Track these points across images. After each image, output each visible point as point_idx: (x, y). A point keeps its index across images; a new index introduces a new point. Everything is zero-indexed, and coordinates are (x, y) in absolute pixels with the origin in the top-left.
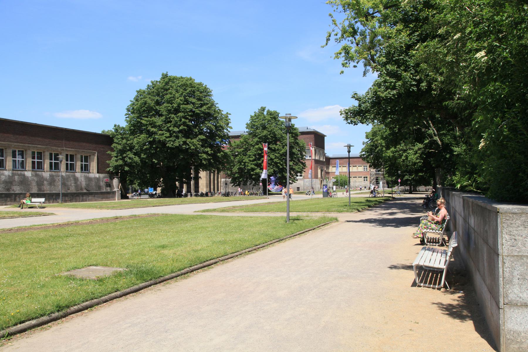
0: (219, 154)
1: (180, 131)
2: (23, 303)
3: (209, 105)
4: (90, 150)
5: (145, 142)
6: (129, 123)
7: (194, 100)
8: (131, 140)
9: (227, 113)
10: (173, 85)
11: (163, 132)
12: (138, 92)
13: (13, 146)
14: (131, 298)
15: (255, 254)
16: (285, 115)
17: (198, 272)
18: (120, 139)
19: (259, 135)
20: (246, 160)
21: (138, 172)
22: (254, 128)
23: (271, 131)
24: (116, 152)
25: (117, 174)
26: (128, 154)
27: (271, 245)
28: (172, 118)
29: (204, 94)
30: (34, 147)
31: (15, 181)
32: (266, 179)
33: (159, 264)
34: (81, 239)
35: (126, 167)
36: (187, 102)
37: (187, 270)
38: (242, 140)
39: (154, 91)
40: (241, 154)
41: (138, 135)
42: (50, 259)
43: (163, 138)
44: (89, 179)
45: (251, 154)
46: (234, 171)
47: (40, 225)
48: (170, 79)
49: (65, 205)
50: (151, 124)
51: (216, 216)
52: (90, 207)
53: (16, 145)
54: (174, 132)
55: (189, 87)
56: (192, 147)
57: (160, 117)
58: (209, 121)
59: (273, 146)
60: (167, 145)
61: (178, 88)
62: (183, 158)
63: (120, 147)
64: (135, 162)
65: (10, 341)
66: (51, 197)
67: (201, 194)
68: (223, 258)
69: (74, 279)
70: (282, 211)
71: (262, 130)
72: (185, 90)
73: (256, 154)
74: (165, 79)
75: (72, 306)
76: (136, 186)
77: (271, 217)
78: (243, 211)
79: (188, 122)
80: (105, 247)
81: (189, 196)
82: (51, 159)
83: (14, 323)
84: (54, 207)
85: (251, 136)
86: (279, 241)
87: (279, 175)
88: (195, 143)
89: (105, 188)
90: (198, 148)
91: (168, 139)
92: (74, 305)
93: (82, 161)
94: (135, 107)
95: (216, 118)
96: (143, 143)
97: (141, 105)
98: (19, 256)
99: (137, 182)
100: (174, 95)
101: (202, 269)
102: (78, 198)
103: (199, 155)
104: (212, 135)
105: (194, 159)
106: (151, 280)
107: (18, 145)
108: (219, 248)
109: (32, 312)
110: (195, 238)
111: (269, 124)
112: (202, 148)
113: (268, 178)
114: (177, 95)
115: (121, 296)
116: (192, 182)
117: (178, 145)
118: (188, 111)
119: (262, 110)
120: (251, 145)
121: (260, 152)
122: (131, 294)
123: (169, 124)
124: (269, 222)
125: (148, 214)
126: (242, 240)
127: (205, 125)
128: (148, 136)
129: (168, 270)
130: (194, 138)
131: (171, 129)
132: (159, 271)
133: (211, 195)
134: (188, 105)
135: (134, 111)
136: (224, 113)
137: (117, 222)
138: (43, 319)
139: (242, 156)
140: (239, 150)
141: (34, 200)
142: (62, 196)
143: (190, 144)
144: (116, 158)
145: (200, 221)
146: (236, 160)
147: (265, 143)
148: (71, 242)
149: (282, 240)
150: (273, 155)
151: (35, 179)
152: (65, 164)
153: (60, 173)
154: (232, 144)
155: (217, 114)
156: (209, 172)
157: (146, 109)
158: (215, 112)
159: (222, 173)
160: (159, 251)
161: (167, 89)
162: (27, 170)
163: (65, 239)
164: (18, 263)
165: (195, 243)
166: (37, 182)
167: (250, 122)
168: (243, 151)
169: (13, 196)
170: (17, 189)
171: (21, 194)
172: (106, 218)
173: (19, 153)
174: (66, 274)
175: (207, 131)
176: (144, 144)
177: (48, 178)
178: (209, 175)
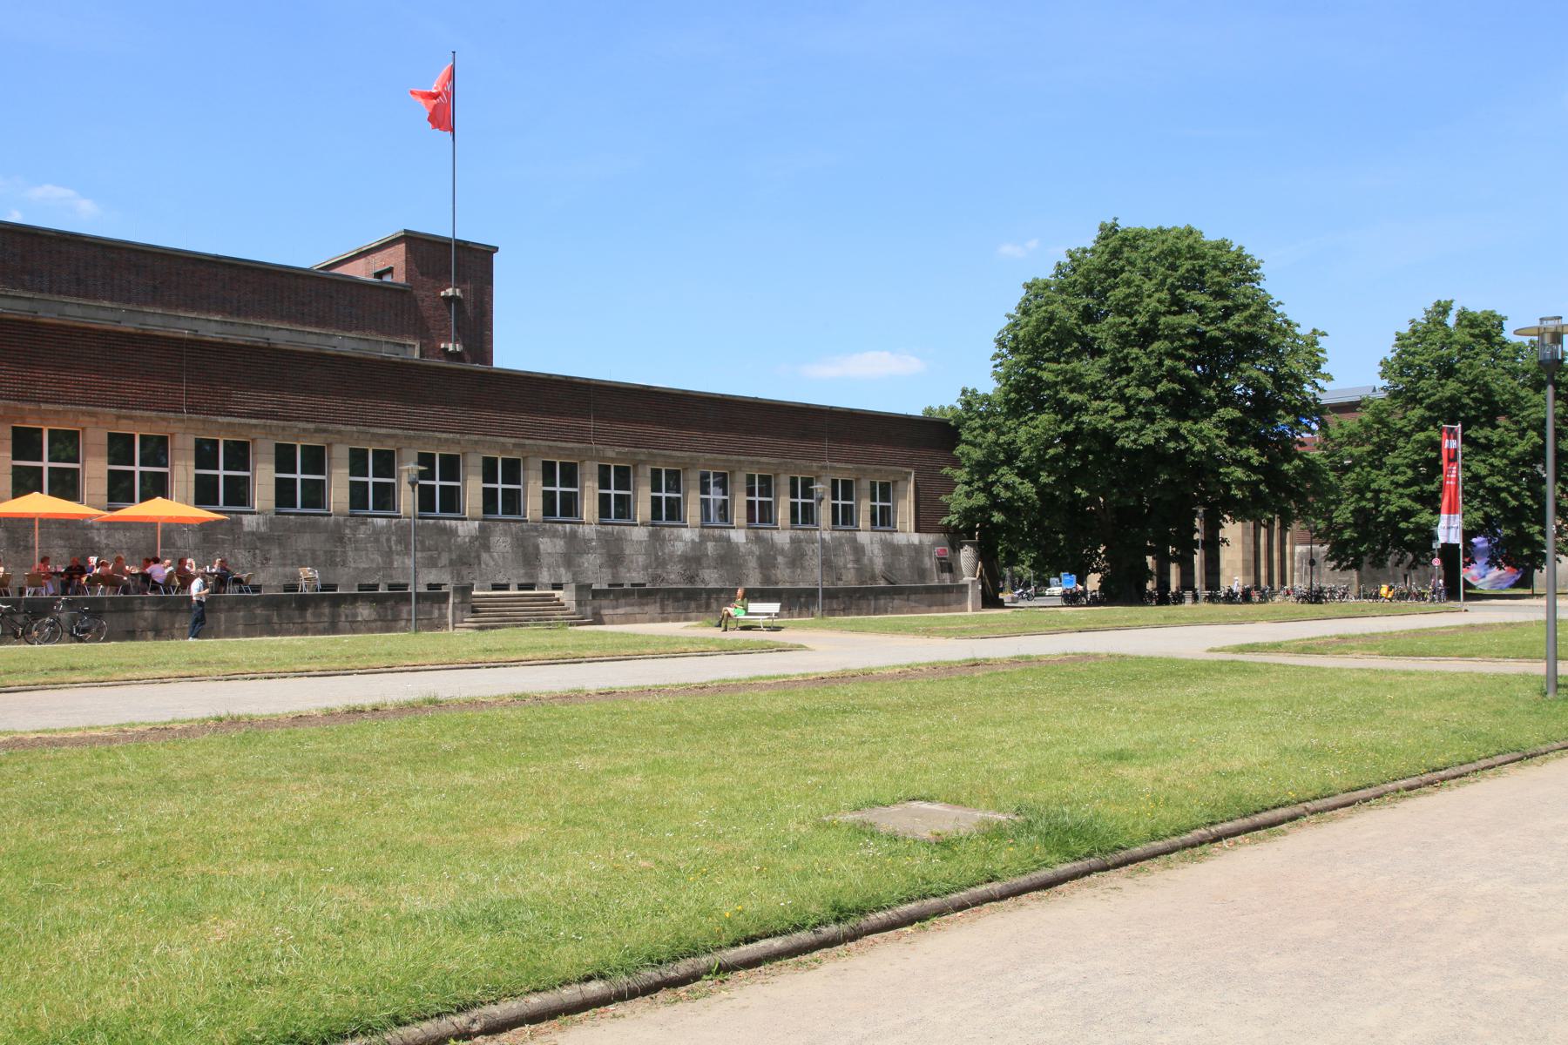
0: (1286, 467)
1: (1160, 399)
2: (751, 890)
3: (1252, 310)
4: (895, 464)
5: (1052, 436)
6: (1004, 381)
7: (1200, 298)
8: (1009, 433)
9: (1314, 330)
10: (1134, 255)
11: (1105, 403)
12: (1028, 287)
13: (702, 461)
14: (1033, 905)
15: (1431, 798)
16: (1537, 323)
17: (1236, 843)
18: (978, 431)
19: (1429, 396)
20: (1382, 481)
21: (1031, 525)
22: (1408, 376)
23: (1473, 381)
24: (967, 470)
25: (969, 532)
26: (1003, 475)
27: (1489, 773)
28: (1133, 359)
29: (1234, 276)
30: (752, 462)
31: (707, 555)
32: (1458, 545)
33: (1110, 810)
34: (882, 718)
35: (995, 514)
36: (1179, 306)
37: (1200, 835)
38: (1366, 416)
39: (1076, 281)
40: (1364, 464)
41: (1031, 415)
42: (806, 773)
43: (1104, 422)
44: (893, 550)
45: (1398, 461)
46: (1339, 520)
47: (774, 677)
48: (1126, 239)
49: (830, 623)
50: (1067, 382)
51: (1286, 666)
52: (897, 630)
53: (708, 460)
54: (1140, 401)
55: (1186, 259)
56: (1199, 447)
57: (1096, 358)
58: (1251, 359)
59: (1480, 434)
60: (1119, 443)
61: (1152, 264)
62: (1171, 481)
63: (977, 454)
64: (1021, 498)
65: (724, 986)
66: (797, 601)
67: (1227, 596)
68: (1318, 804)
69: (872, 835)
70: (1524, 657)
71: (1439, 379)
72: (1173, 267)
73: (1416, 462)
74: (1109, 240)
75: (871, 912)
76: (1025, 570)
77: (1482, 676)
78: (1377, 652)
79: (1185, 368)
80: (950, 748)
81: (1188, 602)
82: (794, 494)
83: (732, 939)
84: (804, 627)
85: (1399, 402)
86: (1521, 759)
87: (1504, 532)
88: (1205, 433)
89: (938, 576)
90: (1217, 448)
91: (1119, 425)
92: (879, 909)
93: (873, 499)
94: (1021, 334)
95: (1275, 349)
96: (1047, 440)
97: (1037, 327)
98: (729, 759)
99: (1027, 557)
100: (1137, 286)
101: (1249, 834)
102: (863, 603)
103: (1221, 470)
104: (1263, 407)
105: (1204, 484)
106: (1090, 855)
107: (715, 460)
108: (1302, 770)
109: (774, 915)
110: (1219, 734)
111: (1467, 357)
112: (1230, 449)
113: (1464, 541)
114: (1148, 286)
115: (1003, 897)
116: (1198, 559)
117: (1152, 441)
118: (1185, 335)
119: (1439, 313)
120: (1400, 431)
121: (1434, 455)
122: (1033, 894)
123: (1125, 377)
124: (1478, 691)
125: (1066, 654)
126: (1382, 747)
127: (1239, 373)
128: (1060, 417)
129: (1142, 830)
130: (1205, 417)
131: (1129, 392)
132: (1113, 832)
133: (1261, 597)
134: (1183, 316)
135: (1018, 344)
136: (1303, 331)
137: (976, 674)
138: (799, 938)
139: (1369, 469)
140: (1357, 451)
141: (754, 607)
142: (823, 598)
143: (1190, 438)
144: (966, 488)
145: (1232, 681)
146: (1347, 484)
147: (1453, 422)
148: (855, 729)
149: (1532, 756)
150: (1484, 461)
151: (756, 549)
152: (830, 507)
153: (818, 533)
154: (1331, 432)
155: (1280, 338)
156: (1251, 524)
157: (1053, 337)
158: (1271, 329)
159: (1296, 526)
160: (1109, 768)
161: (1115, 271)
162: (735, 525)
163: (839, 719)
164: (728, 779)
165: (1220, 750)
166: (759, 558)
167: (1394, 354)
168: (1370, 453)
169: (704, 596)
170: (711, 578)
171: (721, 591)
172: (945, 663)
173: (717, 479)
174: (851, 817)
175: (1246, 393)
176: (1049, 444)
177: (787, 547)
178: (1252, 533)
